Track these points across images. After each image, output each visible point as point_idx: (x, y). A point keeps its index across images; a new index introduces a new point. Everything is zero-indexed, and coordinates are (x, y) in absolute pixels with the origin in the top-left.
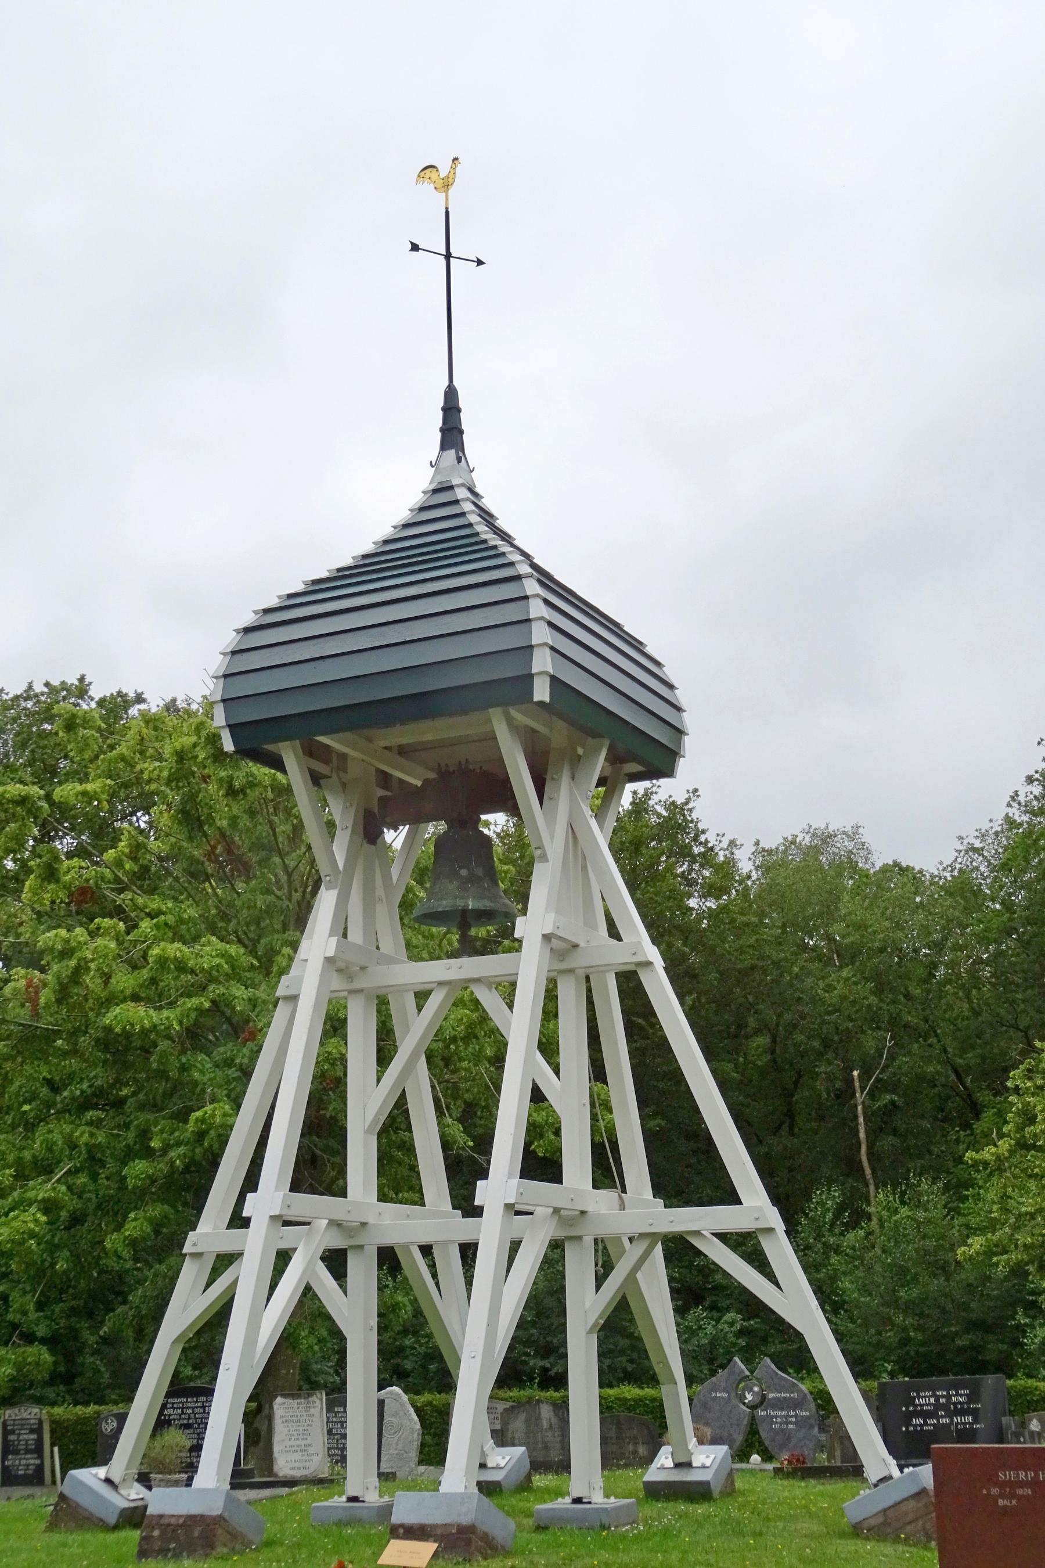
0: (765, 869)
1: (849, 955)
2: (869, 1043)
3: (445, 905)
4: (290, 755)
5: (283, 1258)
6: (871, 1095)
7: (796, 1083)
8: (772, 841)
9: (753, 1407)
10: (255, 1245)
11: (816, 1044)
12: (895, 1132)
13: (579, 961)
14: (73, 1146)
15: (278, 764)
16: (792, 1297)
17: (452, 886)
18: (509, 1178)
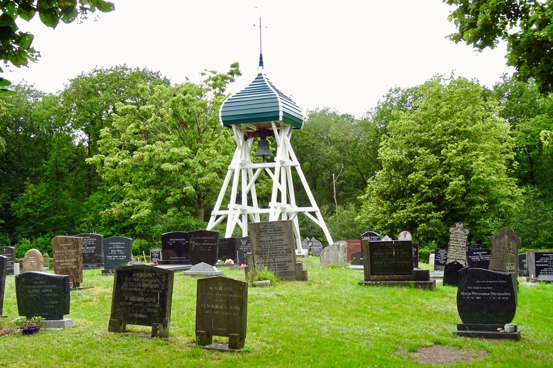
0: (310, 116)
1: (333, 142)
2: (337, 166)
3: (261, 154)
4: (234, 127)
6: (337, 181)
7: (317, 177)
8: (313, 109)
9: (310, 247)
11: (323, 167)
12: (343, 190)
13: (285, 164)
14: (150, 194)
16: (321, 222)
17: (262, 150)
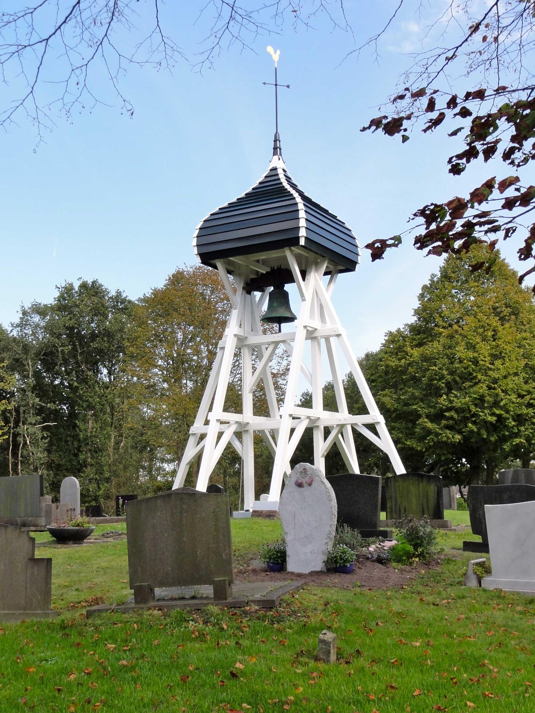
5: (220, 435)
10: (212, 430)
15: (215, 267)
18: (274, 155)
